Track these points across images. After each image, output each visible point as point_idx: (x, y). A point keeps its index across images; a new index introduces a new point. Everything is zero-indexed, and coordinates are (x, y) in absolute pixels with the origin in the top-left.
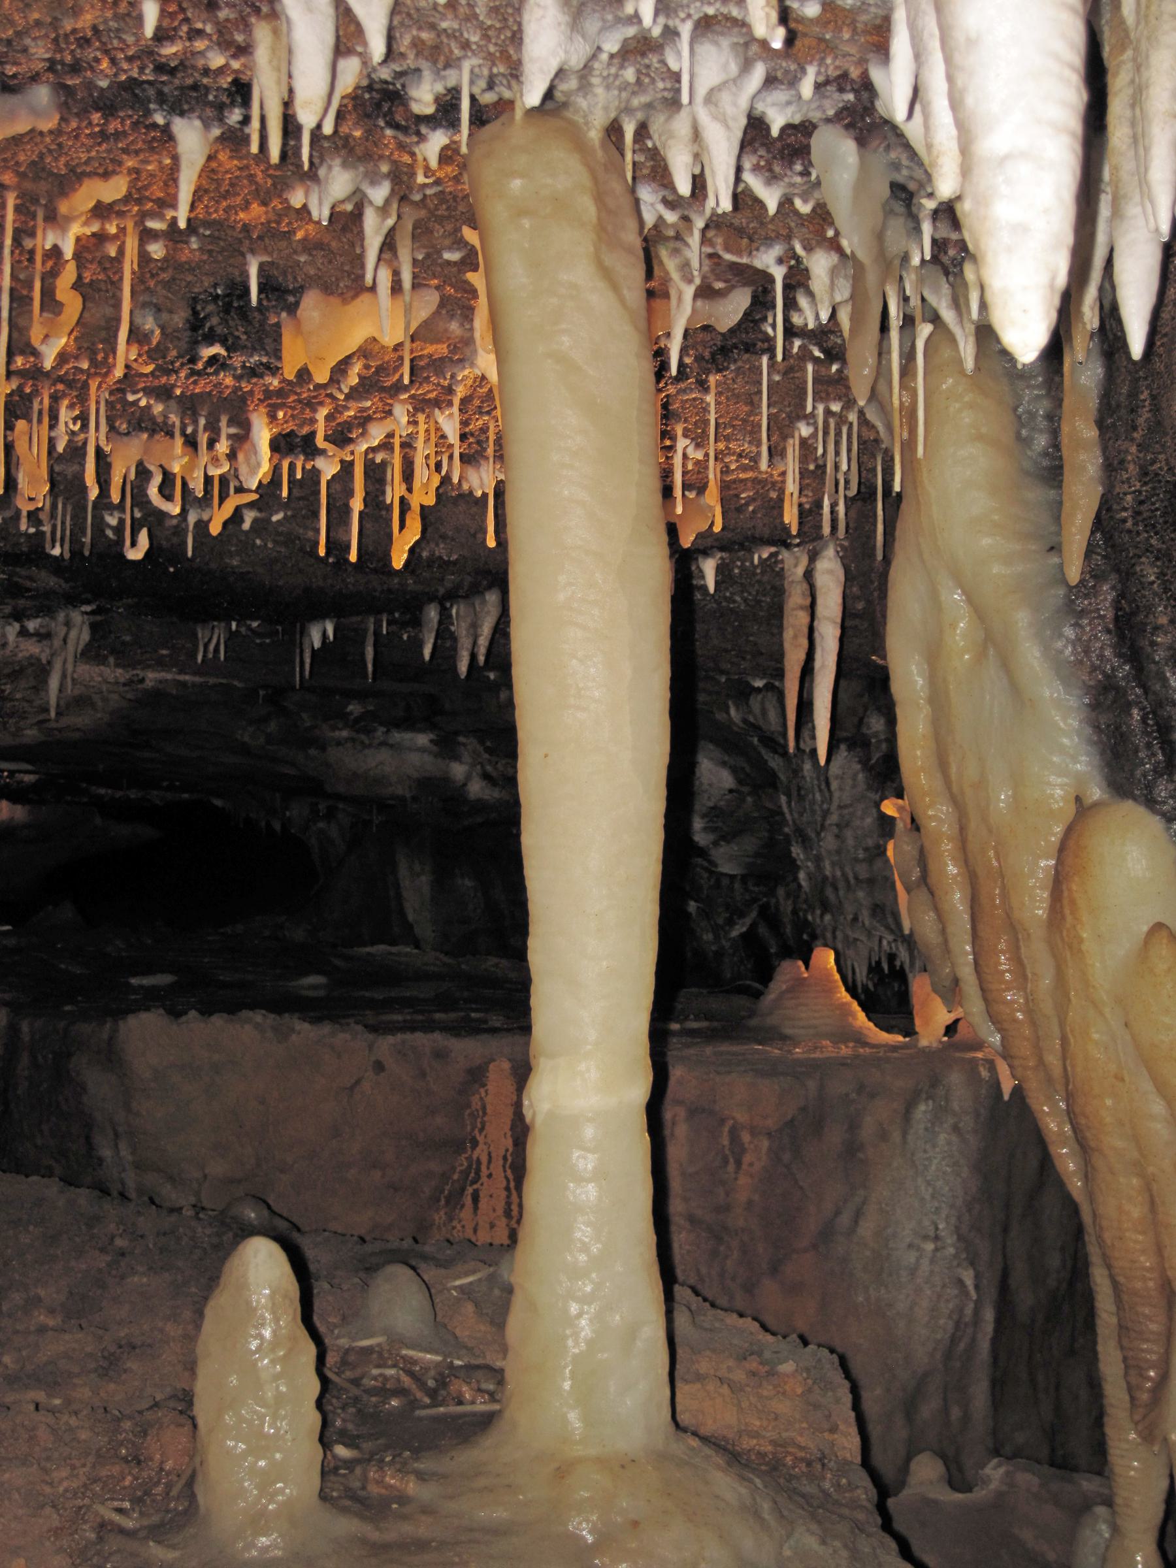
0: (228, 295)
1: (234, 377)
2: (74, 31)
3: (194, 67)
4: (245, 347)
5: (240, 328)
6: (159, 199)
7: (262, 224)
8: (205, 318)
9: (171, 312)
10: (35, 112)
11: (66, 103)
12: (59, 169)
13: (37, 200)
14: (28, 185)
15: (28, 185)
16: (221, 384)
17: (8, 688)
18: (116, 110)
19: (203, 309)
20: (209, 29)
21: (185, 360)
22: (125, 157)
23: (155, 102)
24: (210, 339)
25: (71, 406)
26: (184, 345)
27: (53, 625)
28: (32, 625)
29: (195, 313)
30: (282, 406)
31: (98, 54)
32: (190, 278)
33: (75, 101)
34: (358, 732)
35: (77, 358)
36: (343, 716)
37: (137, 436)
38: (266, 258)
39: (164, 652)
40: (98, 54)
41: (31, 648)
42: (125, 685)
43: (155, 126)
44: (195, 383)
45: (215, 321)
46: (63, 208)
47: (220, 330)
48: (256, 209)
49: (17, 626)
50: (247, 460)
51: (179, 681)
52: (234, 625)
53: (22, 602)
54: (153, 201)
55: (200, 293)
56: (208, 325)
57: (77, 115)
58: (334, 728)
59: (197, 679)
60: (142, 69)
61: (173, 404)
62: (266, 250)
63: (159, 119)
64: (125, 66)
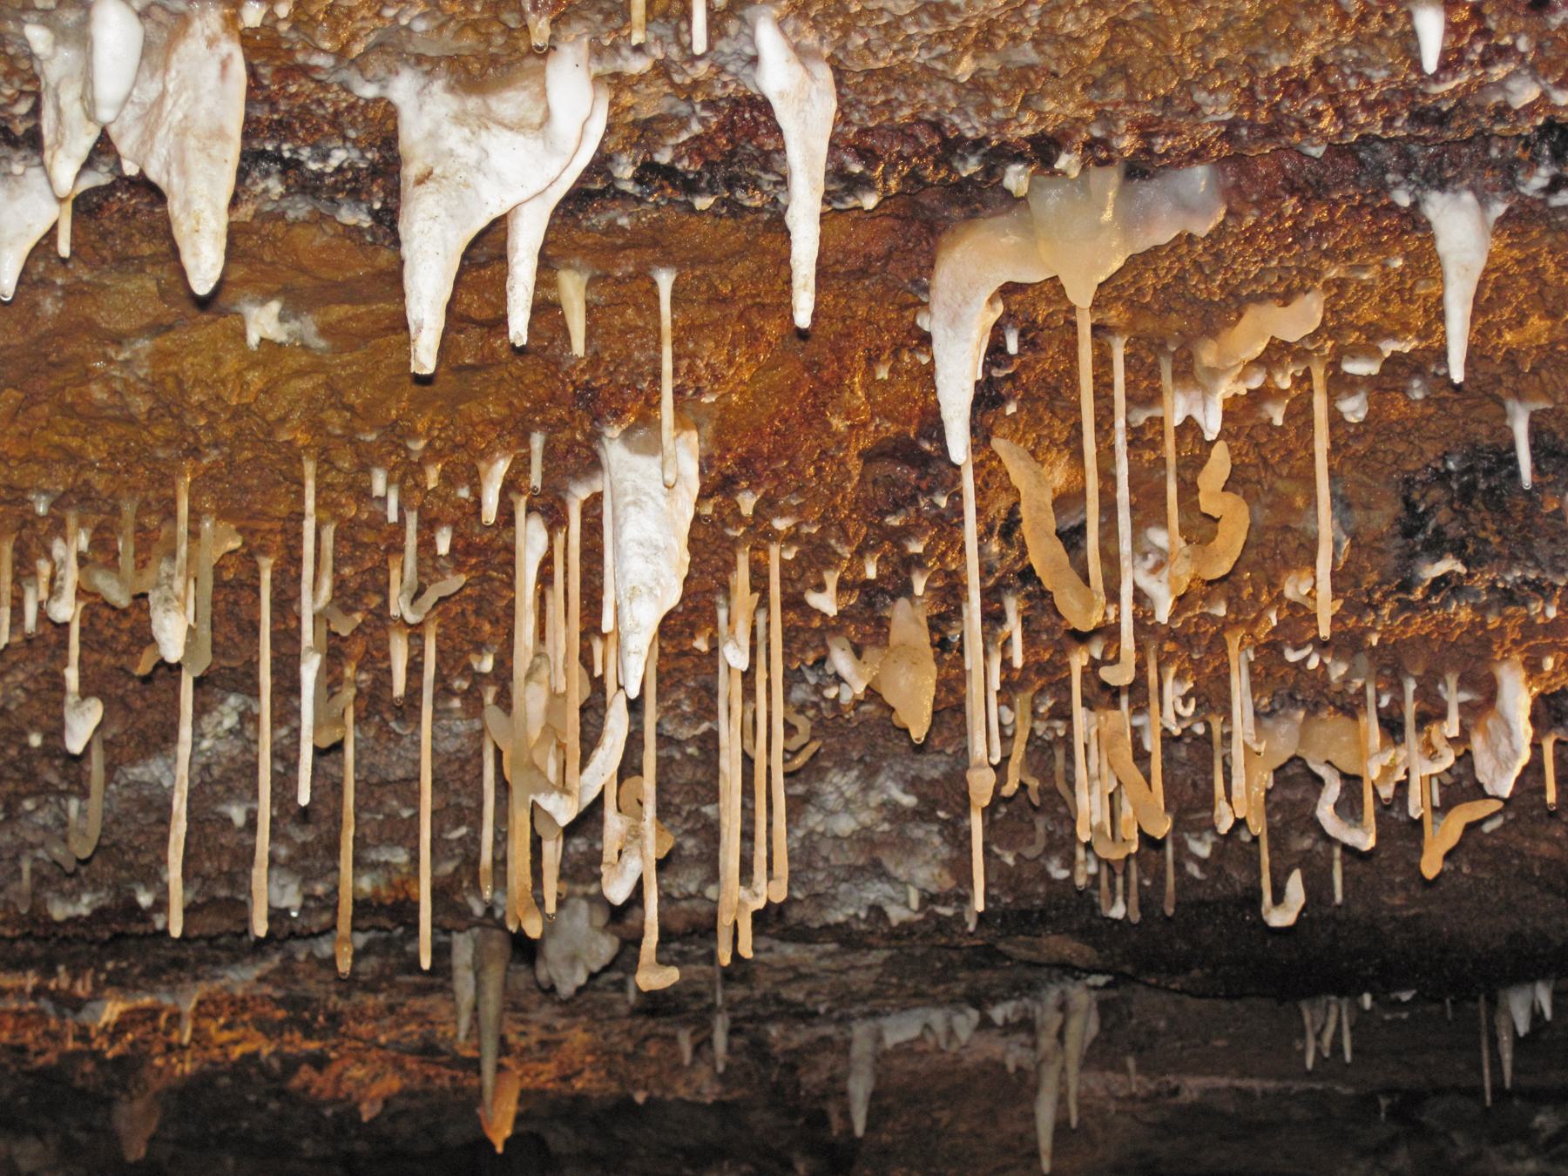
0: (1471, 470)
1: (1475, 608)
2: (1285, 70)
3: (1480, 109)
4: (1498, 556)
5: (1489, 525)
6: (1370, 324)
7: (1539, 347)
8: (1425, 512)
9: (1367, 507)
10: (1185, 207)
11: (1237, 187)
12: (1211, 294)
13: (1163, 346)
14: (1148, 324)
15: (1148, 324)
16: (1450, 621)
17: (945, 1116)
18: (1327, 189)
19: (1423, 496)
20: (1523, 44)
21: (1393, 587)
22: (1326, 263)
23: (1396, 170)
24: (1436, 548)
25: (1179, 677)
26: (1391, 562)
27: (1038, 1010)
28: (998, 1013)
29: (1410, 505)
30: (1551, 649)
31: (1320, 106)
32: (1401, 448)
33: (1254, 181)
34: (1553, 1160)
35: (1206, 598)
36: (1527, 1134)
37: (1286, 716)
38: (1542, 405)
39: (1220, 1043)
40: (1320, 106)
41: (994, 1047)
42: (1144, 1100)
43: (1392, 207)
44: (1406, 622)
45: (1443, 515)
46: (1207, 355)
47: (1454, 530)
48: (1537, 324)
49: (974, 1015)
50: (1493, 748)
51: (1238, 1089)
52: (1367, 1000)
53: (985, 977)
54: (1359, 329)
55: (1416, 472)
56: (1432, 524)
57: (1257, 204)
58: (1511, 1157)
59: (1271, 1085)
60: (1389, 122)
61: (1362, 660)
62: (1544, 392)
63: (1403, 199)
64: (1362, 118)
